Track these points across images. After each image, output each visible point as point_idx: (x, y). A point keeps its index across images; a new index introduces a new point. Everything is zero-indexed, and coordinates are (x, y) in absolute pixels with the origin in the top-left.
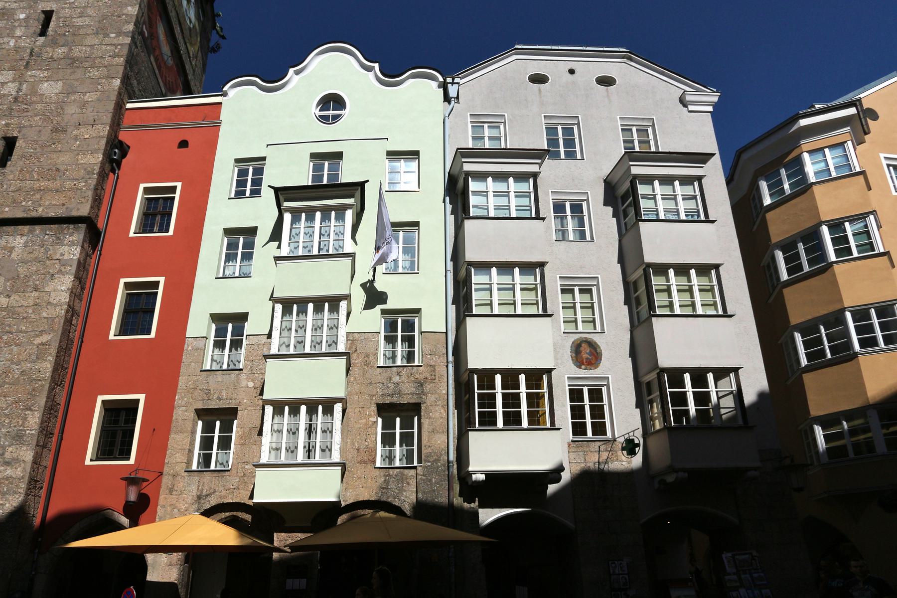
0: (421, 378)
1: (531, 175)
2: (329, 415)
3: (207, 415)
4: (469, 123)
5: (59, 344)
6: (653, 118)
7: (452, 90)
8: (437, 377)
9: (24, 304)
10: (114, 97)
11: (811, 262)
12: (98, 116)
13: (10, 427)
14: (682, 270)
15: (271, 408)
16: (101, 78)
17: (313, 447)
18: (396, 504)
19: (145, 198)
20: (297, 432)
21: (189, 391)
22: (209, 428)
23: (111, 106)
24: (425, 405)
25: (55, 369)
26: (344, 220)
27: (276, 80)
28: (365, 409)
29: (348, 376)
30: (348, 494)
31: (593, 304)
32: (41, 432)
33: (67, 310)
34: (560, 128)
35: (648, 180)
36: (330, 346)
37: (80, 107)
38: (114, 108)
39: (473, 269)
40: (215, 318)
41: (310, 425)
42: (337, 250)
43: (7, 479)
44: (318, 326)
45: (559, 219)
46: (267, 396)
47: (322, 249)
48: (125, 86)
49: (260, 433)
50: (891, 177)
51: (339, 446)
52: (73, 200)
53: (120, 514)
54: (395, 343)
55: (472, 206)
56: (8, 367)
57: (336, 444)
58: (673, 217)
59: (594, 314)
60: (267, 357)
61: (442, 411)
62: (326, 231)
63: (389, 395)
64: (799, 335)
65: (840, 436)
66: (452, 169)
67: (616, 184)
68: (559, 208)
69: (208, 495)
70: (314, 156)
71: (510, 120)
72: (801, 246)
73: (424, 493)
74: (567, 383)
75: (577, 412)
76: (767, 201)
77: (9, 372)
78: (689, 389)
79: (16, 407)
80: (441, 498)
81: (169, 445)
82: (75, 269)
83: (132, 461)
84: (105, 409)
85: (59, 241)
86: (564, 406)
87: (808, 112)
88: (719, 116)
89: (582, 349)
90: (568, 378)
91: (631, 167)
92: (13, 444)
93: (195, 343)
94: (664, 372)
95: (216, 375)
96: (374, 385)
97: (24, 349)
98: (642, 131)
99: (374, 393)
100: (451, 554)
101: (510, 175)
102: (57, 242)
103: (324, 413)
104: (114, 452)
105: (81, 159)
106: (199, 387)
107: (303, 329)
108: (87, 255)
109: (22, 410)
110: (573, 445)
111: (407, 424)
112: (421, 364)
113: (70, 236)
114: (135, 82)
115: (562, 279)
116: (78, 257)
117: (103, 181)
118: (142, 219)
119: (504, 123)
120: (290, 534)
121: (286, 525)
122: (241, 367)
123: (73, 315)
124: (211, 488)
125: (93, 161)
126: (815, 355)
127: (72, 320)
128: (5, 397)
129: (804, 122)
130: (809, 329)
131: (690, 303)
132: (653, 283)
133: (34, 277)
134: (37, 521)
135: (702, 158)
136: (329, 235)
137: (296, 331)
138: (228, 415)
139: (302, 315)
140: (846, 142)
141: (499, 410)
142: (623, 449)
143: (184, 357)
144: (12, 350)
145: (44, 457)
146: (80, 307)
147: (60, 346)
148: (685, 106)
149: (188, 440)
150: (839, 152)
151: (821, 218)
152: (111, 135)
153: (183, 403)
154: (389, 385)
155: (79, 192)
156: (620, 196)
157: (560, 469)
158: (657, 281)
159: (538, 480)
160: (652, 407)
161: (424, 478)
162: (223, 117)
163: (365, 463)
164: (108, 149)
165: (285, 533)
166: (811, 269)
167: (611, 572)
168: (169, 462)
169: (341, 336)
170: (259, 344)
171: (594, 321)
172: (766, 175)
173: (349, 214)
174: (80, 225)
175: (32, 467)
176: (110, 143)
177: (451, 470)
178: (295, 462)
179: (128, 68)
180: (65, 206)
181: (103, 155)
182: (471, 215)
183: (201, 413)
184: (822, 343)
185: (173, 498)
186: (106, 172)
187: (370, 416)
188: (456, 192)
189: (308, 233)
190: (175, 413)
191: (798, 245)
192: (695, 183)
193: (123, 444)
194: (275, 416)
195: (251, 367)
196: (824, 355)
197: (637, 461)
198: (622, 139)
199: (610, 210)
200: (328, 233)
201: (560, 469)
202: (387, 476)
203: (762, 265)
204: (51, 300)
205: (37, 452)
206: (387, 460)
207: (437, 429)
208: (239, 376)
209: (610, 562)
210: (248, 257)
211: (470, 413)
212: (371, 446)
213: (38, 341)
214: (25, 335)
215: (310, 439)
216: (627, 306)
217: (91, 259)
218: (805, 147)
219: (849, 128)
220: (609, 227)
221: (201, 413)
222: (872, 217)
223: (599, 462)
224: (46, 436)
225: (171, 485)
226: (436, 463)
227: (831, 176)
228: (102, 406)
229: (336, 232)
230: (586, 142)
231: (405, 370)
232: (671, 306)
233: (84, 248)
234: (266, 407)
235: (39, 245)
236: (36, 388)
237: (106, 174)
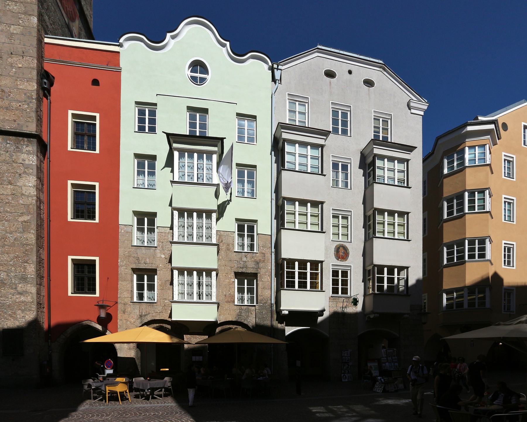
0: (258, 259)
1: (320, 145)
2: (209, 277)
3: (140, 272)
4: (287, 100)
5: (37, 223)
6: (392, 114)
7: (277, 74)
8: (266, 260)
9: (4, 193)
10: (35, 33)
11: (458, 211)
12: (25, 48)
13: (16, 272)
14: (391, 213)
15: (177, 271)
16: (20, 13)
17: (201, 293)
18: (246, 323)
19: (74, 121)
20: (192, 285)
21: (126, 258)
22: (140, 279)
23: (35, 42)
24: (260, 274)
25: (37, 239)
26: (211, 160)
27: (160, 41)
28: (228, 274)
29: (218, 256)
30: (221, 317)
31: (348, 225)
32: (38, 276)
33: (37, 200)
34: (340, 111)
35: (382, 158)
36: (207, 238)
37: (8, 38)
38: (37, 44)
39: (286, 202)
40: (136, 213)
41: (199, 282)
42: (209, 180)
43: (23, 302)
44: (200, 226)
45: (335, 172)
46: (174, 265)
47: (199, 178)
48: (41, 23)
49: (172, 283)
50: (505, 167)
51: (216, 294)
52: (21, 118)
53: (95, 323)
54: (244, 238)
55: (287, 161)
56: (5, 235)
57: (214, 293)
58: (391, 182)
59: (348, 232)
60: (172, 243)
61: (268, 278)
62: (201, 167)
63: (241, 268)
64: (446, 248)
65: (452, 299)
66: (276, 132)
67: (367, 155)
68: (335, 166)
69: (145, 315)
70: (189, 108)
71: (311, 102)
72: (455, 201)
73: (259, 318)
74: (331, 267)
75: (335, 282)
76: (446, 171)
77: (6, 238)
78: (386, 275)
79: (17, 260)
80: (268, 321)
81: (119, 287)
82: (36, 172)
83: (97, 295)
84: (74, 264)
85: (19, 150)
86: (329, 279)
87: (472, 123)
88: (427, 119)
89: (340, 250)
90: (332, 265)
91: (374, 148)
92: (21, 283)
93: (126, 228)
94: (375, 266)
95: (141, 249)
96: (233, 262)
97: (12, 224)
98: (385, 122)
99: (233, 266)
100: (272, 347)
101: (308, 144)
102: (17, 150)
103: (206, 276)
104: (85, 289)
105: (20, 85)
106: (132, 255)
107: (191, 227)
108: (41, 161)
109: (22, 262)
110: (331, 298)
111: (250, 283)
112: (258, 252)
113: (26, 147)
114: (46, 18)
115: (333, 210)
116: (36, 163)
117: (40, 104)
118: (74, 137)
119: (308, 103)
120: (192, 336)
121: (190, 331)
122: (156, 246)
123: (40, 204)
124: (147, 311)
125: (30, 88)
126: (450, 260)
127: (40, 206)
128: (7, 254)
129: (470, 128)
130: (450, 246)
131: (393, 232)
132: (377, 219)
133: (6, 174)
134: (45, 326)
135: (410, 149)
136: (203, 169)
137: (188, 228)
138: (152, 273)
139: (190, 218)
140: (486, 144)
141: (297, 280)
142: (352, 302)
143: (120, 237)
144: (4, 224)
145: (42, 290)
146: (44, 197)
147: (37, 224)
148: (410, 109)
149: (129, 285)
150: (481, 150)
151: (466, 187)
152: (39, 67)
153: (124, 264)
154: (241, 262)
155: (24, 112)
156: (368, 163)
157: (324, 310)
158: (379, 218)
159: (315, 314)
160: (369, 282)
161: (259, 311)
162: (122, 64)
163: (229, 302)
164: (39, 78)
165: (190, 335)
166: (457, 215)
167: (343, 355)
168: (120, 296)
169: (214, 234)
170: (166, 233)
171: (347, 235)
172: (448, 155)
173: (215, 157)
174: (32, 139)
175: (37, 297)
176: (40, 74)
177: (272, 308)
178: (193, 301)
179: (40, 6)
180: (16, 123)
181: (37, 84)
182: (286, 168)
183: (135, 270)
184: (454, 254)
185: (126, 316)
186: (41, 97)
187: (231, 278)
188: (278, 149)
189: (190, 166)
190: (119, 269)
191: (454, 200)
192: (405, 163)
193: (89, 285)
194: (179, 276)
195: (162, 246)
196: (454, 260)
197: (359, 308)
198: (373, 125)
199: (361, 171)
200: (202, 168)
201: (324, 310)
202: (240, 309)
203: (439, 207)
204: (24, 192)
205: (38, 288)
206: (241, 300)
207: (266, 287)
208: (155, 251)
209: (343, 351)
210: (152, 174)
211: (282, 281)
212: (232, 294)
213: (21, 219)
214: (10, 214)
215: (199, 289)
216: (364, 229)
217: (44, 163)
218: (468, 144)
219: (489, 136)
220: (360, 182)
221: (135, 270)
222: (488, 191)
223: (342, 307)
224: (40, 278)
225: (123, 309)
226: (265, 304)
227: (475, 164)
228: (72, 262)
229: (207, 168)
230: (353, 126)
231: (249, 255)
232: (383, 232)
233: (38, 157)
234: (174, 271)
235: (4, 151)
236: (27, 249)
237: (41, 98)
